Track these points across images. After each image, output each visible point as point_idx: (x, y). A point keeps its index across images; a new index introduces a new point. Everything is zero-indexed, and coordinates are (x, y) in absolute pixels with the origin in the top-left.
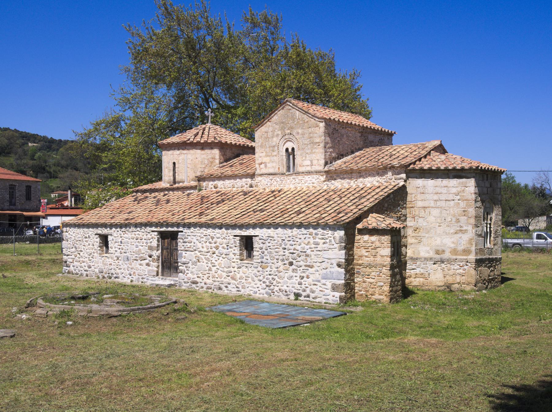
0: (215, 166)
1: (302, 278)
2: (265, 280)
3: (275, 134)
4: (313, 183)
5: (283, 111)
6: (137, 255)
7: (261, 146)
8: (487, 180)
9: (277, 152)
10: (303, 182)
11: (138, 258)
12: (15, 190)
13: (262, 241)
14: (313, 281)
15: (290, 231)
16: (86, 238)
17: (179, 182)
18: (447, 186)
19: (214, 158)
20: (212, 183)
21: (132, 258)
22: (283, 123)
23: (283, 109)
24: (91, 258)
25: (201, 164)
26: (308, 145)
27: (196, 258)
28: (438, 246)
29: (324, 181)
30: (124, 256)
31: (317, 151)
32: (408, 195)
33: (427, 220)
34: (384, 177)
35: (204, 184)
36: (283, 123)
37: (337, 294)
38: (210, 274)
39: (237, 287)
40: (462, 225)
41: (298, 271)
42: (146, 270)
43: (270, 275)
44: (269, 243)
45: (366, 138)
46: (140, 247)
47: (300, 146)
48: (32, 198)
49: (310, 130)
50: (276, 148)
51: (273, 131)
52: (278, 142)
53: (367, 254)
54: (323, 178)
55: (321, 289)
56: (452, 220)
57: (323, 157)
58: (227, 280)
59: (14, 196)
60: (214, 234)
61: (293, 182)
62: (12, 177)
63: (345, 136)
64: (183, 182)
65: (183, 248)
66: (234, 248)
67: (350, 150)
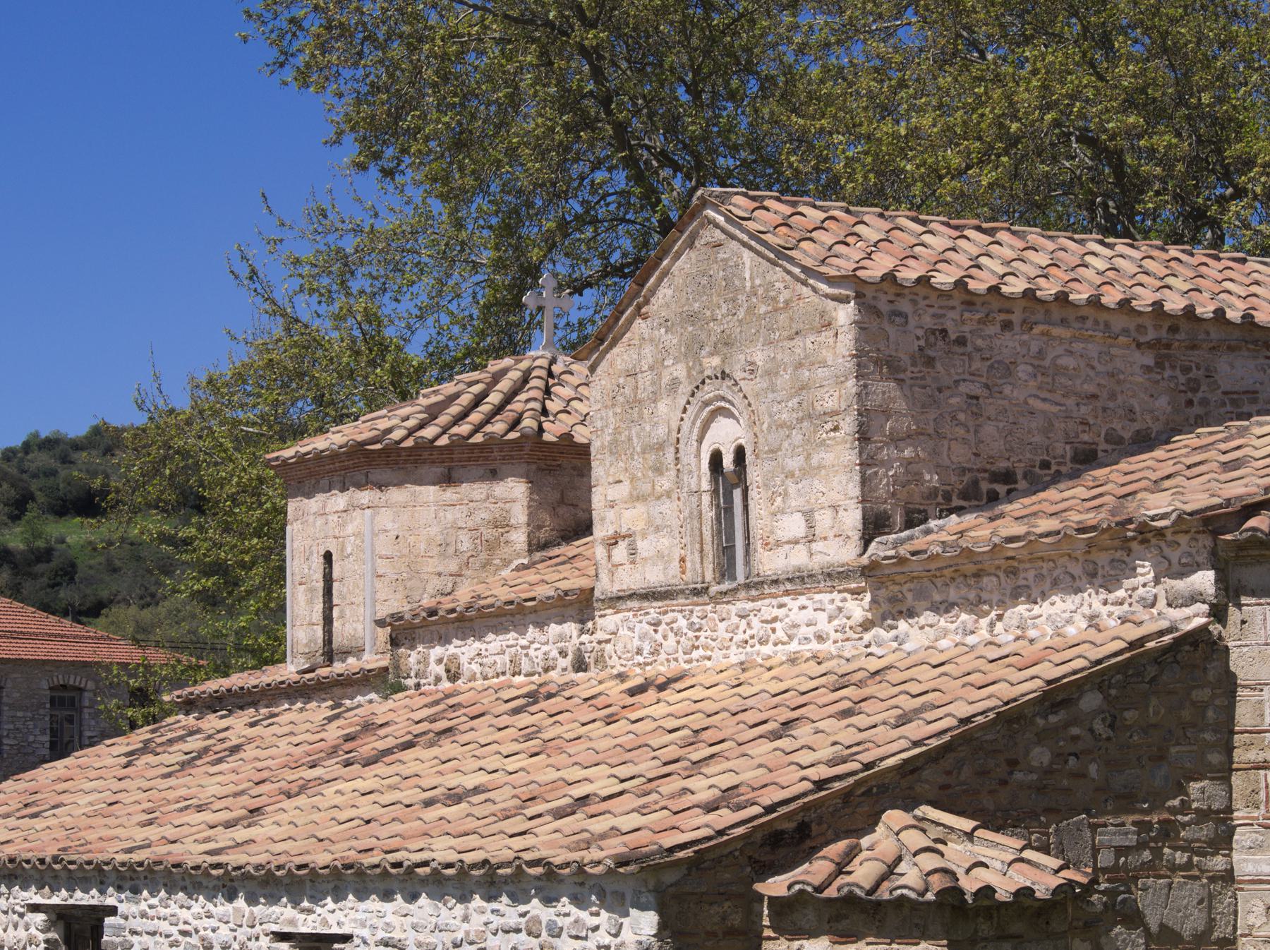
0: (506, 563)
4: (820, 638)
5: (693, 255)
7: (614, 448)
9: (673, 473)
10: (780, 634)
15: (459, 909)
17: (347, 653)
19: (501, 524)
20: (437, 651)
22: (692, 318)
23: (691, 244)
25: (443, 555)
29: (866, 626)
32: (1240, 692)
34: (1121, 593)
35: (412, 658)
36: (692, 318)
47: (761, 440)
50: (670, 452)
52: (674, 426)
54: (858, 609)
57: (855, 491)
61: (740, 637)
62: (67, 652)
63: (1023, 371)
64: (358, 651)
67: (1063, 449)
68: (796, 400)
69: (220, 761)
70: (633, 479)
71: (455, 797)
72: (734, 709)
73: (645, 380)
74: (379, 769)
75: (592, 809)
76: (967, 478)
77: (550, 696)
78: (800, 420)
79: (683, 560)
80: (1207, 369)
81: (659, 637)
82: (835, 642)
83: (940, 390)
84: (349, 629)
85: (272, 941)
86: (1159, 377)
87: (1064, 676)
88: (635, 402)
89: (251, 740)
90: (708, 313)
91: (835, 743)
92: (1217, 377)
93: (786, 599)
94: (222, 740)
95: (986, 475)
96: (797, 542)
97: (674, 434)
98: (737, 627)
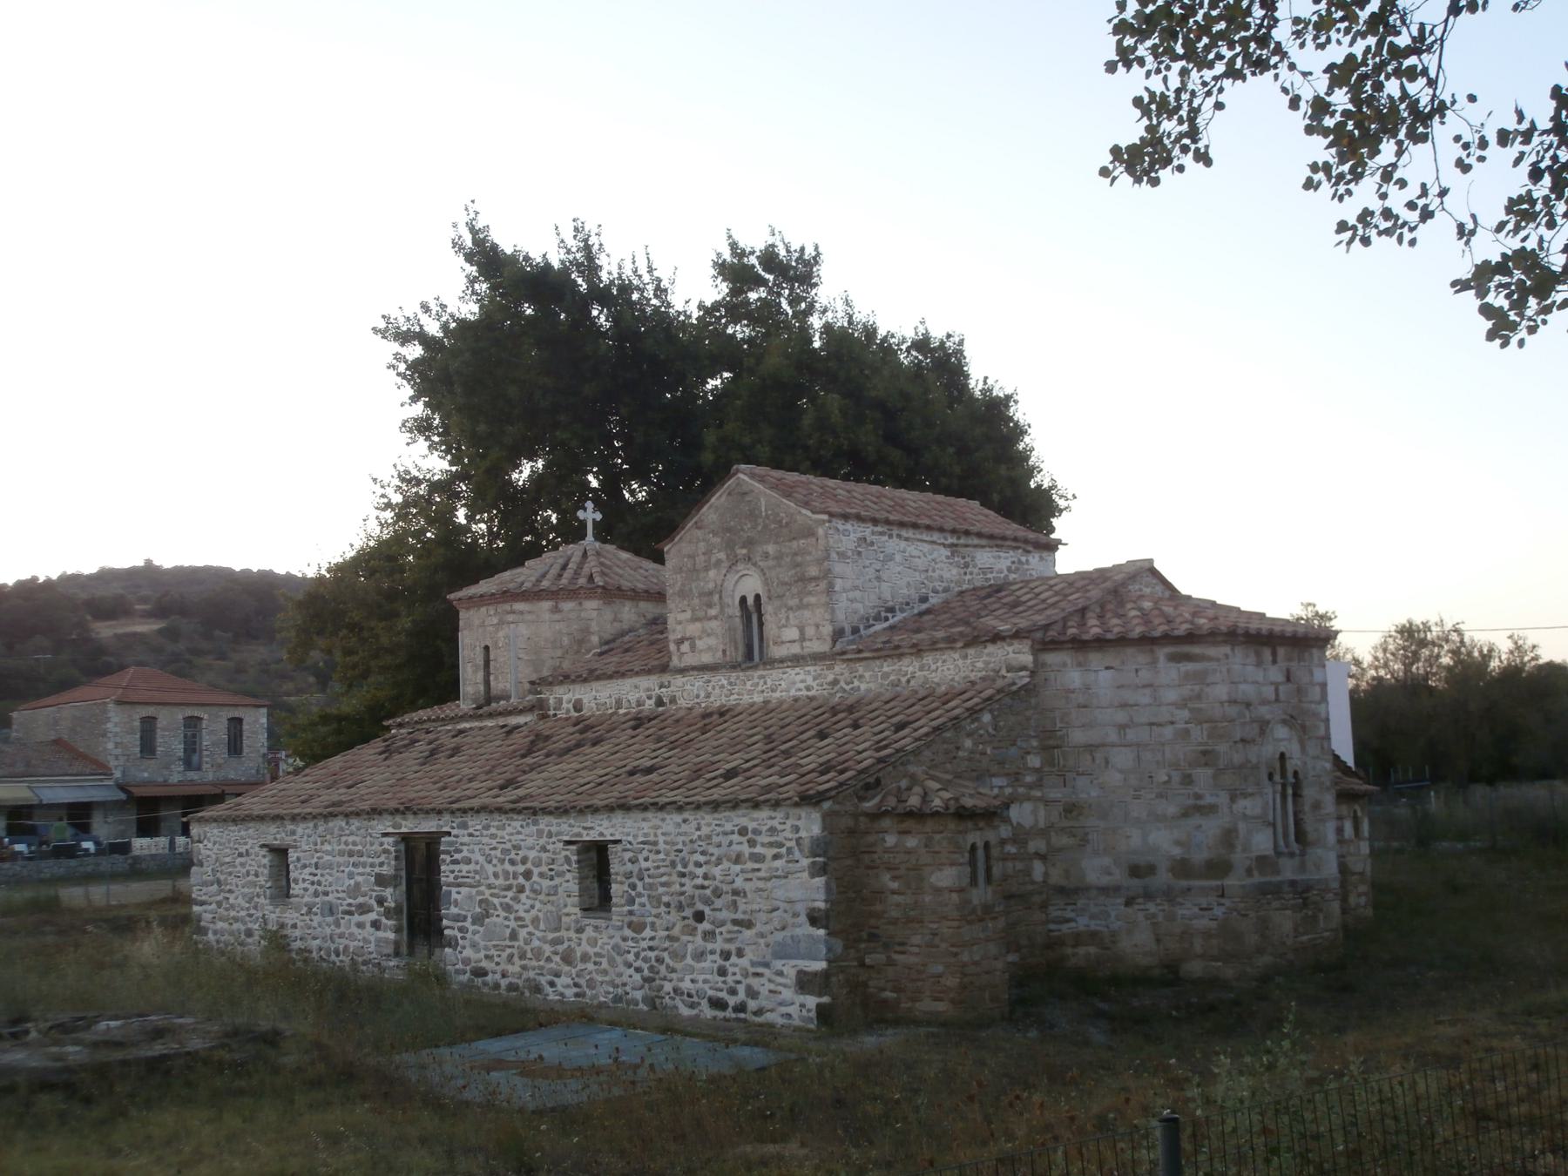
0: (588, 651)
1: (726, 955)
2: (639, 963)
3: (713, 560)
4: (808, 688)
6: (351, 901)
7: (682, 594)
8: (1274, 662)
11: (353, 909)
12: (200, 731)
13: (630, 854)
14: (753, 964)
16: (240, 855)
17: (498, 698)
18: (1150, 685)
21: (341, 908)
22: (729, 530)
24: (252, 911)
26: (790, 585)
27: (480, 907)
30: (323, 903)
31: (812, 600)
36: (729, 530)
37: (811, 1001)
38: (513, 947)
39: (576, 985)
40: (1200, 792)
41: (718, 937)
42: (372, 939)
43: (651, 949)
44: (646, 859)
45: (968, 559)
46: (360, 879)
47: (772, 591)
48: (246, 750)
49: (794, 544)
50: (716, 597)
51: (708, 553)
52: (719, 583)
53: (895, 885)
55: (772, 987)
56: (1170, 777)
58: (552, 965)
59: (197, 746)
60: (521, 837)
61: (760, 688)
65: (451, 879)
66: (568, 876)
68: (793, 572)
76: (876, 610)
78: (796, 582)
81: (710, 689)
84: (501, 686)
96: (794, 641)
97: (719, 587)
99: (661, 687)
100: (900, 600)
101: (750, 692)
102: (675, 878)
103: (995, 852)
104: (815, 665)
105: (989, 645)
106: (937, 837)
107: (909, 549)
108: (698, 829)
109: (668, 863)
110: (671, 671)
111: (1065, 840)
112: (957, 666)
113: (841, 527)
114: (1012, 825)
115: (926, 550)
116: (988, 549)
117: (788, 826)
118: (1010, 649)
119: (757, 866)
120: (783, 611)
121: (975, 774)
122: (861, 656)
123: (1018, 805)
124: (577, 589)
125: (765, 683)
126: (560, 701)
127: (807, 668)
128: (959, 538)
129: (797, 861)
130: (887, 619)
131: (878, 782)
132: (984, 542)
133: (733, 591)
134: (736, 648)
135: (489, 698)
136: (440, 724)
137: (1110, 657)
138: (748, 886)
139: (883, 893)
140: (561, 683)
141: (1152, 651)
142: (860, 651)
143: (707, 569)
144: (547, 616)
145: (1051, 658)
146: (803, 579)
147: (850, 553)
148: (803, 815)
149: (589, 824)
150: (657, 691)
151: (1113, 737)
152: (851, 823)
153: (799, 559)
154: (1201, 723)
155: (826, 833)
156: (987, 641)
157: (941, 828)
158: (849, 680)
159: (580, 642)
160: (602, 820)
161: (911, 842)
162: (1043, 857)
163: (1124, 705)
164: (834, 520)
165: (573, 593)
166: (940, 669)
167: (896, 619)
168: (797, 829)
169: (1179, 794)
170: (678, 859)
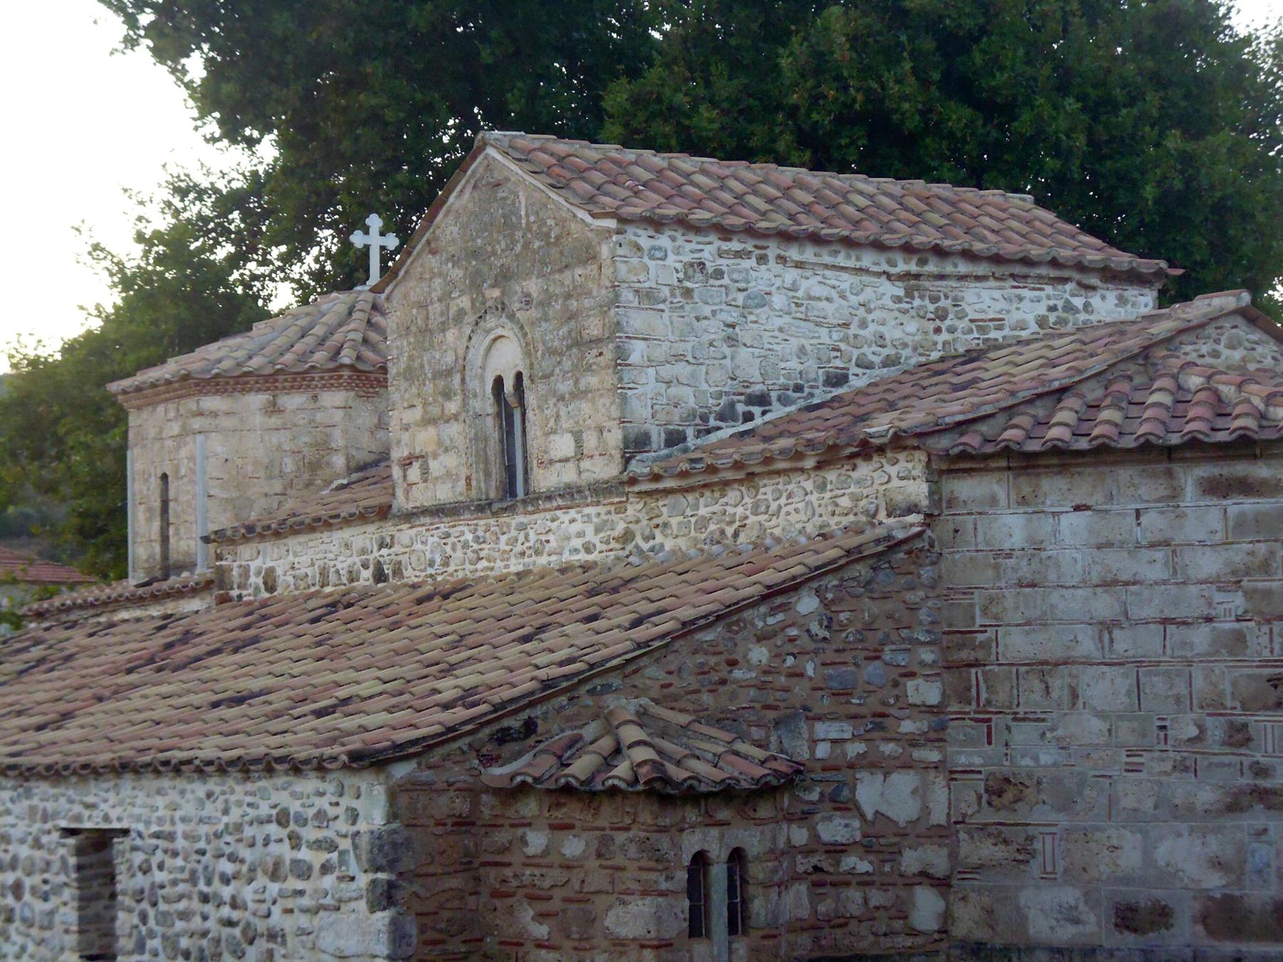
4: (588, 549)
7: (410, 375)
17: (180, 567)
18: (1167, 543)
22: (475, 254)
28: (1127, 880)
33: (1060, 732)
36: (475, 254)
47: (536, 366)
50: (457, 379)
51: (446, 297)
52: (461, 352)
56: (1202, 729)
61: (519, 548)
68: (565, 329)
69: (52, 670)
70: (425, 405)
71: (239, 700)
72: (500, 614)
73: (436, 308)
74: (184, 675)
75: (350, 708)
76: (723, 401)
77: (350, 605)
78: (569, 347)
79: (468, 479)
80: (955, 299)
81: (448, 548)
82: (601, 552)
83: (698, 319)
84: (183, 545)
85: (62, 837)
86: (909, 306)
87: (784, 582)
88: (426, 331)
89: (84, 649)
90: (489, 249)
91: (572, 646)
92: (964, 305)
93: (559, 513)
94: (62, 650)
95: (742, 398)
97: (461, 361)
98: (517, 540)
99: (381, 546)
100: (782, 380)
101: (505, 555)
102: (196, 904)
103: (757, 871)
104: (598, 503)
105: (859, 461)
106: (621, 837)
107: (804, 285)
108: (226, 812)
109: (185, 875)
110: (395, 516)
111: (987, 850)
112: (809, 503)
113: (645, 242)
114: (862, 816)
115: (845, 286)
116: (992, 283)
117: (339, 811)
118: (893, 471)
119: (300, 885)
120: (552, 401)
121: (771, 715)
122: (661, 486)
123: (880, 777)
124: (306, 372)
125: (527, 539)
126: (246, 572)
127: (587, 510)
128: (922, 262)
129: (353, 879)
130: (749, 417)
131: (530, 727)
132: (981, 269)
133: (483, 368)
134: (487, 474)
135: (168, 568)
136: (91, 612)
137: (1084, 486)
138: (288, 924)
139: (522, 945)
140: (245, 539)
141: (1170, 474)
142: (656, 478)
143: (443, 328)
144: (258, 419)
145: (966, 488)
146: (579, 342)
147: (666, 292)
148: (364, 787)
149: (90, 799)
150: (376, 554)
151: (1087, 645)
152: (462, 806)
153: (574, 304)
154: (1268, 622)
155: (395, 825)
156: (852, 456)
157: (628, 821)
158: (647, 532)
159: (314, 467)
160: (107, 791)
161: (573, 846)
162: (942, 884)
163: (1109, 584)
164: (631, 230)
165: (302, 379)
166: (784, 510)
167: (768, 417)
168: (354, 816)
169: (1222, 765)
170: (200, 868)
